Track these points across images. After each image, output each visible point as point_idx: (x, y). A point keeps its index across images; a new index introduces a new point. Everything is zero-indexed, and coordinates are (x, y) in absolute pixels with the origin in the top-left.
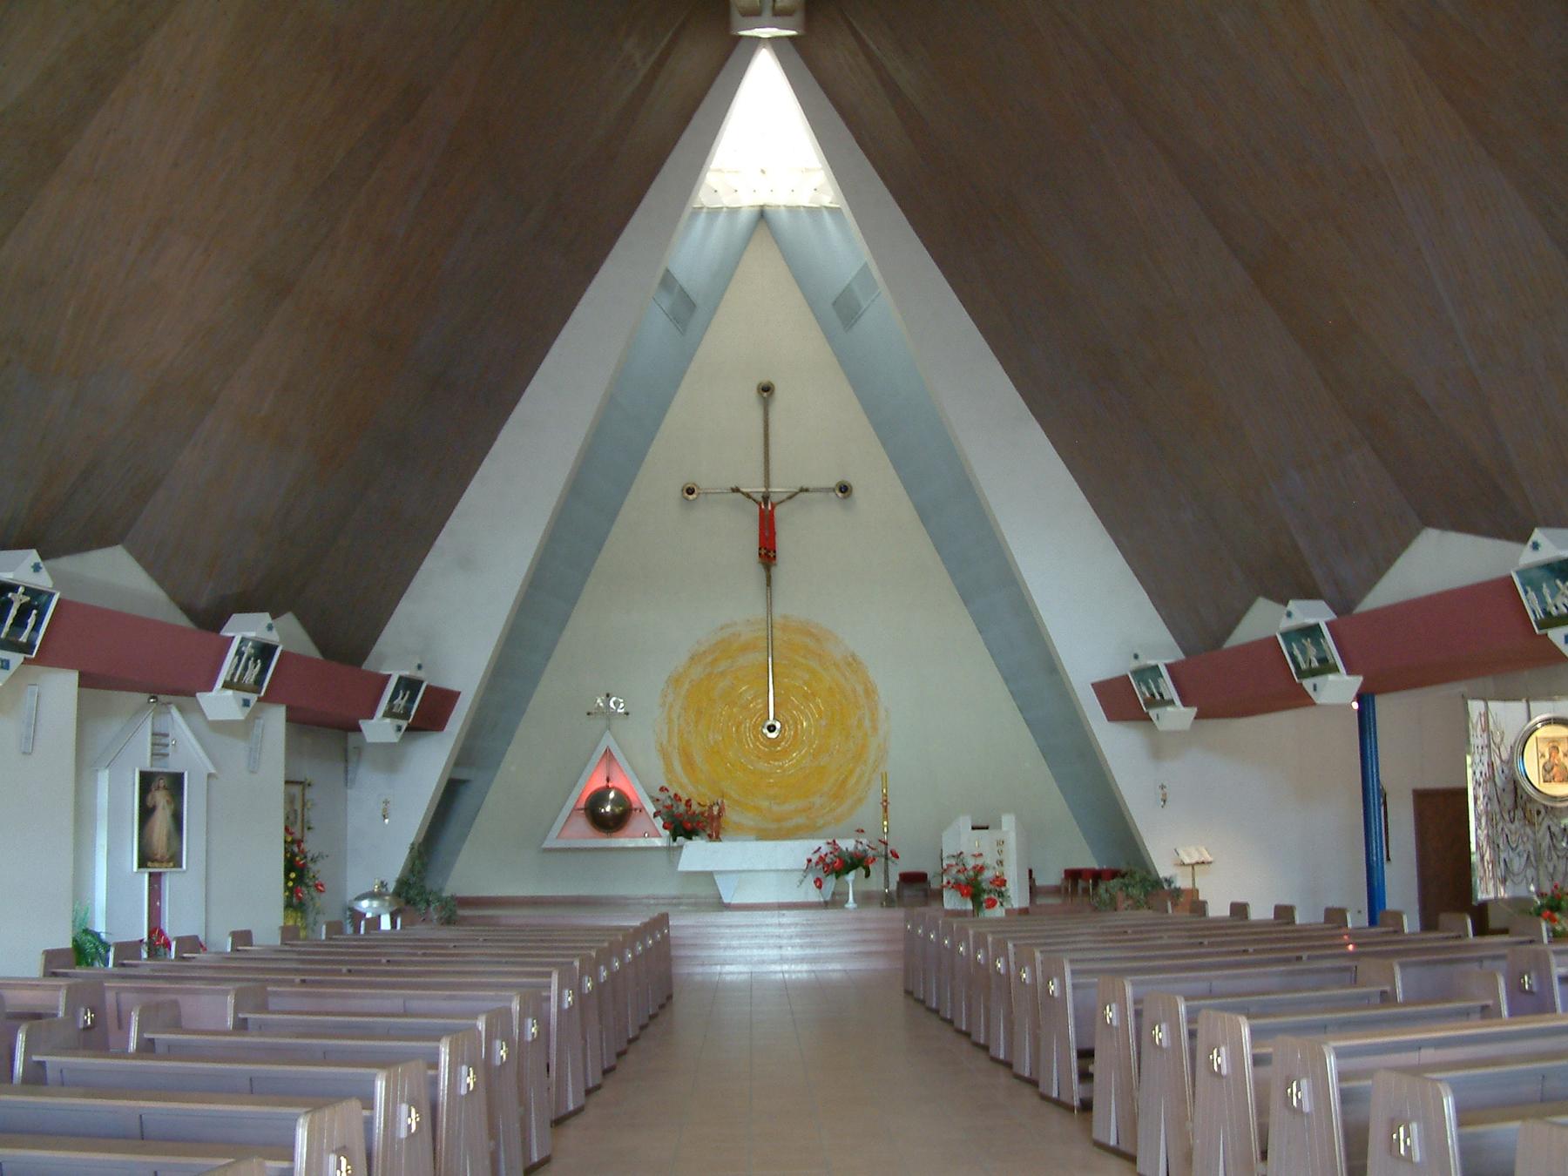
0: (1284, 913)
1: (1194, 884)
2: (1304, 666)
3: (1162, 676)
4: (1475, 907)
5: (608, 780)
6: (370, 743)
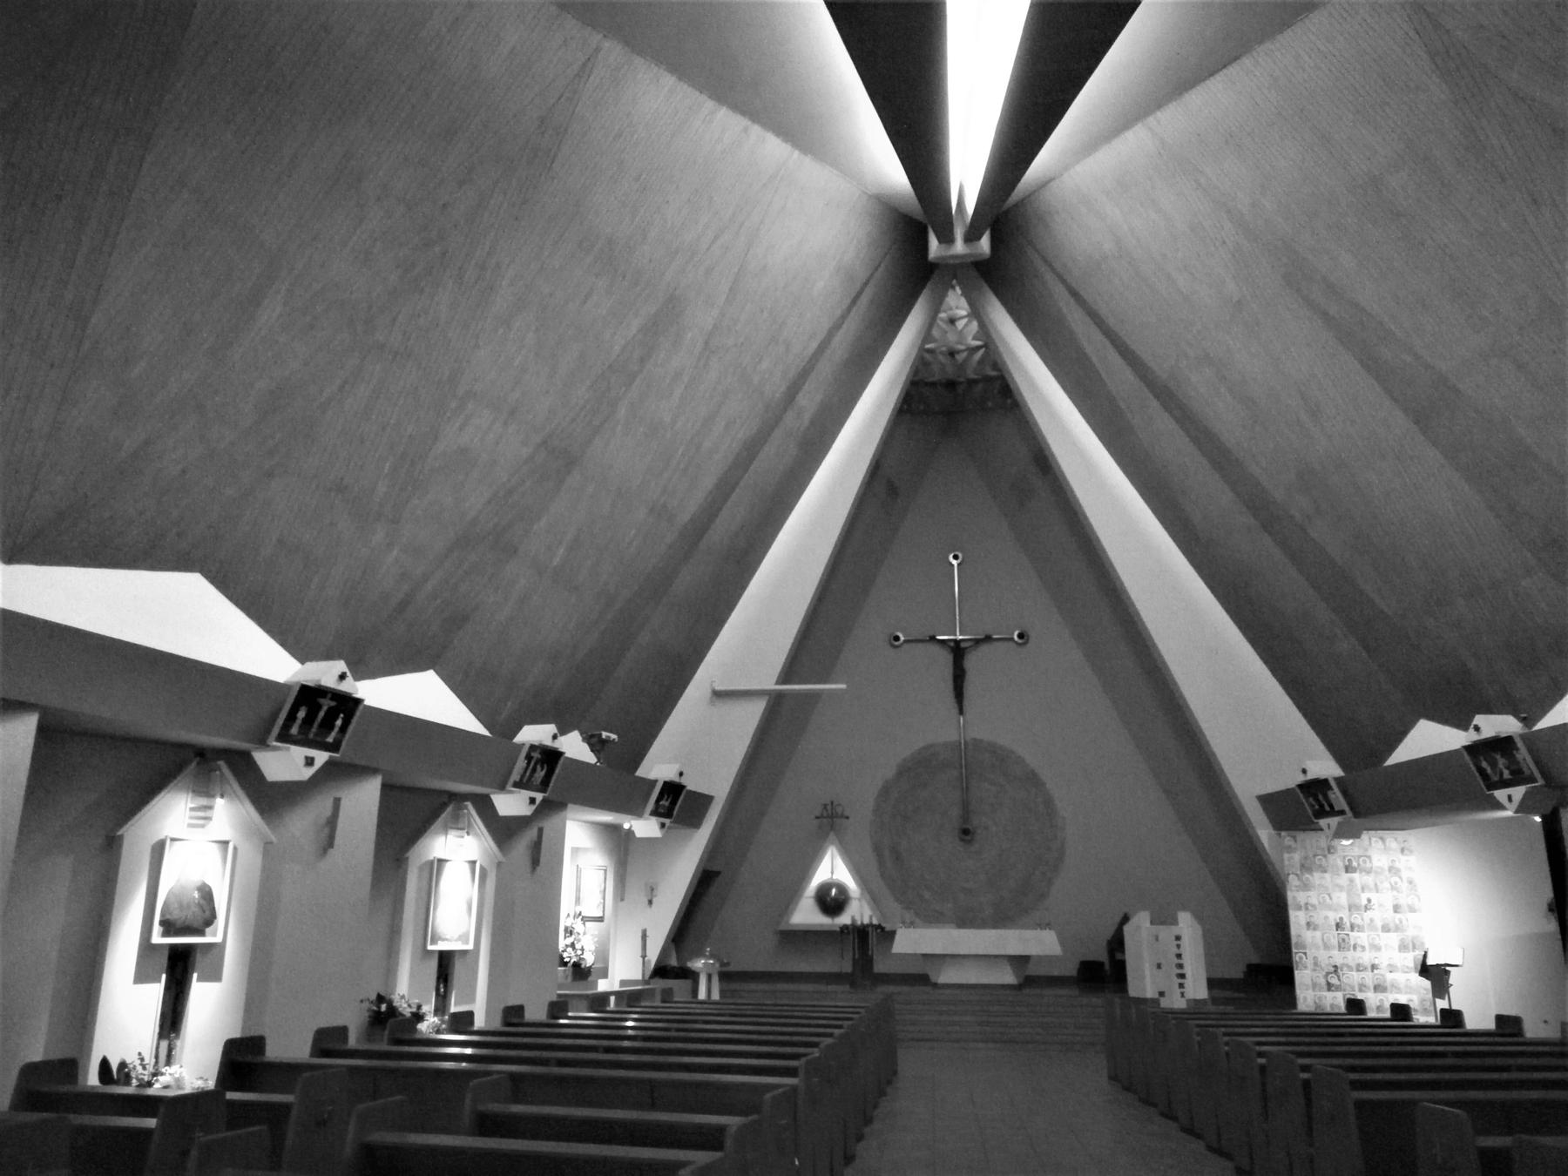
0: (1508, 1025)
1: (1450, 1005)
2: (1496, 778)
3: (1332, 790)
4: (302, 706)
5: (832, 873)
6: (639, 838)
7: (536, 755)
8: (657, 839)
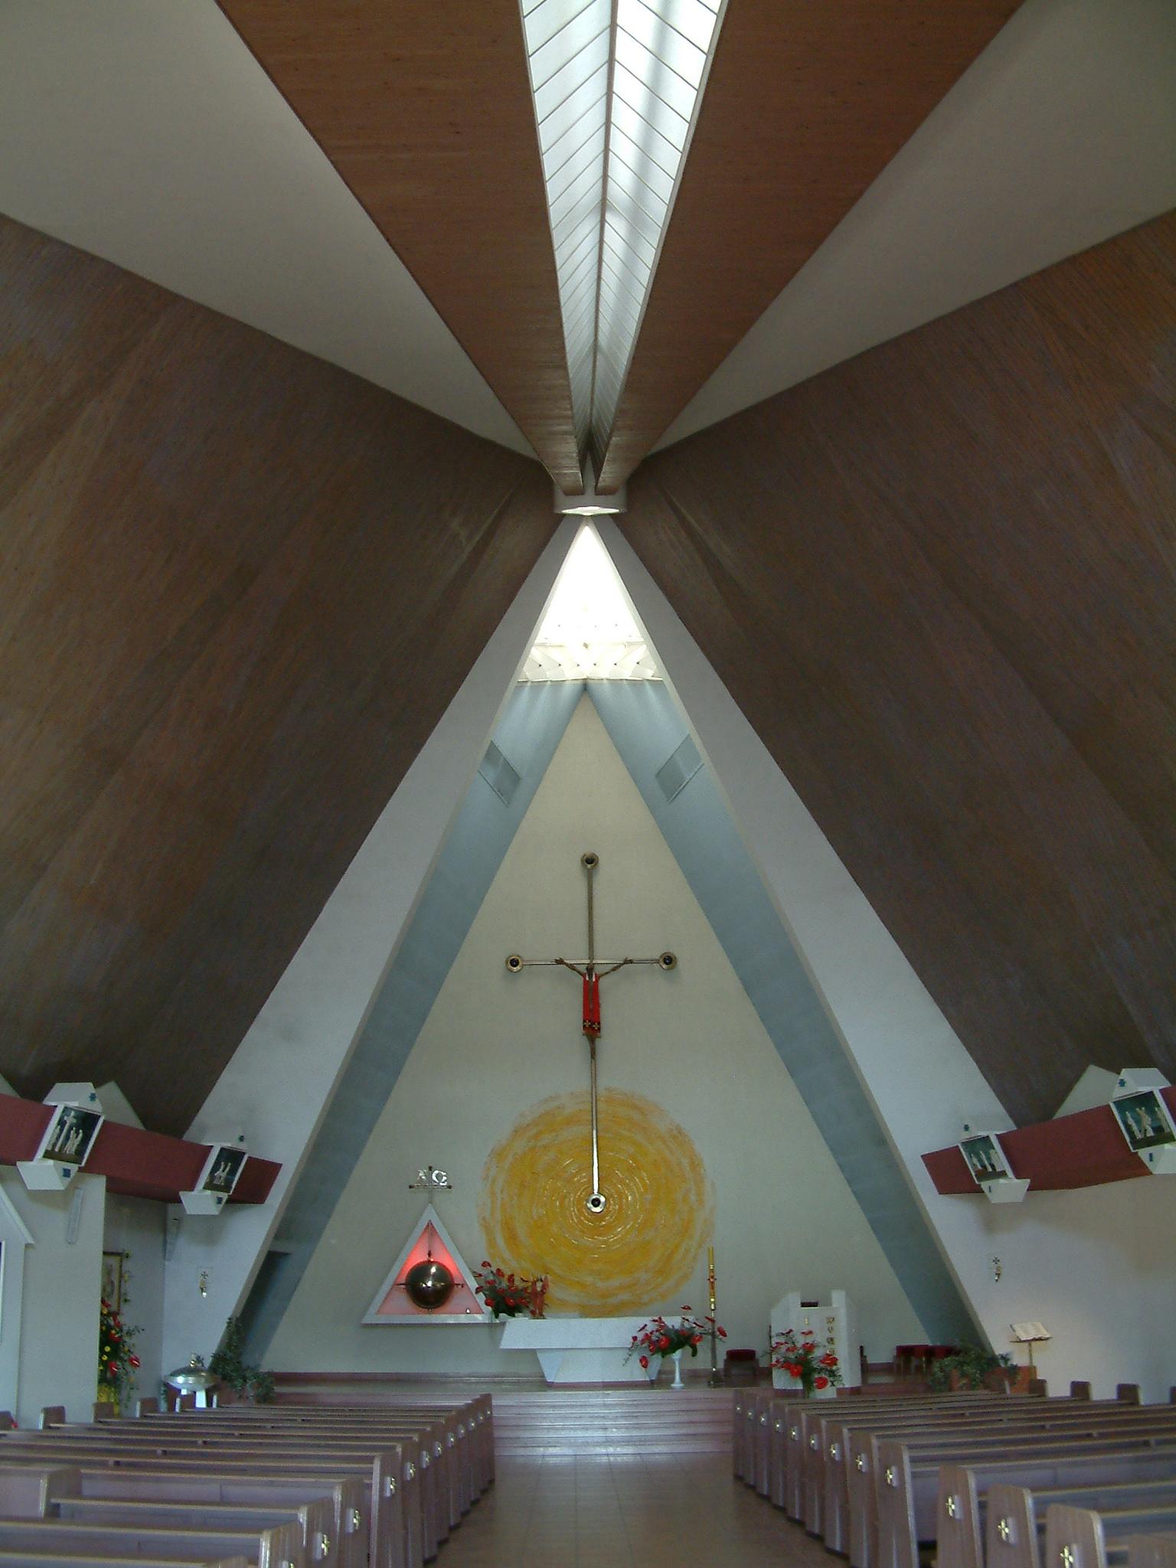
2: (1139, 1136)
7: (70, 1120)
8: (213, 1216)
